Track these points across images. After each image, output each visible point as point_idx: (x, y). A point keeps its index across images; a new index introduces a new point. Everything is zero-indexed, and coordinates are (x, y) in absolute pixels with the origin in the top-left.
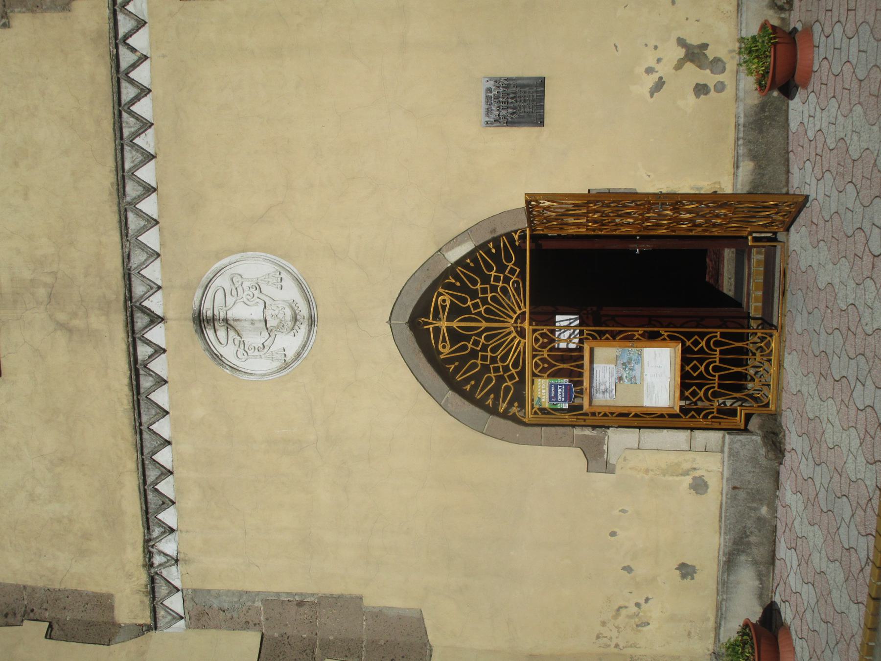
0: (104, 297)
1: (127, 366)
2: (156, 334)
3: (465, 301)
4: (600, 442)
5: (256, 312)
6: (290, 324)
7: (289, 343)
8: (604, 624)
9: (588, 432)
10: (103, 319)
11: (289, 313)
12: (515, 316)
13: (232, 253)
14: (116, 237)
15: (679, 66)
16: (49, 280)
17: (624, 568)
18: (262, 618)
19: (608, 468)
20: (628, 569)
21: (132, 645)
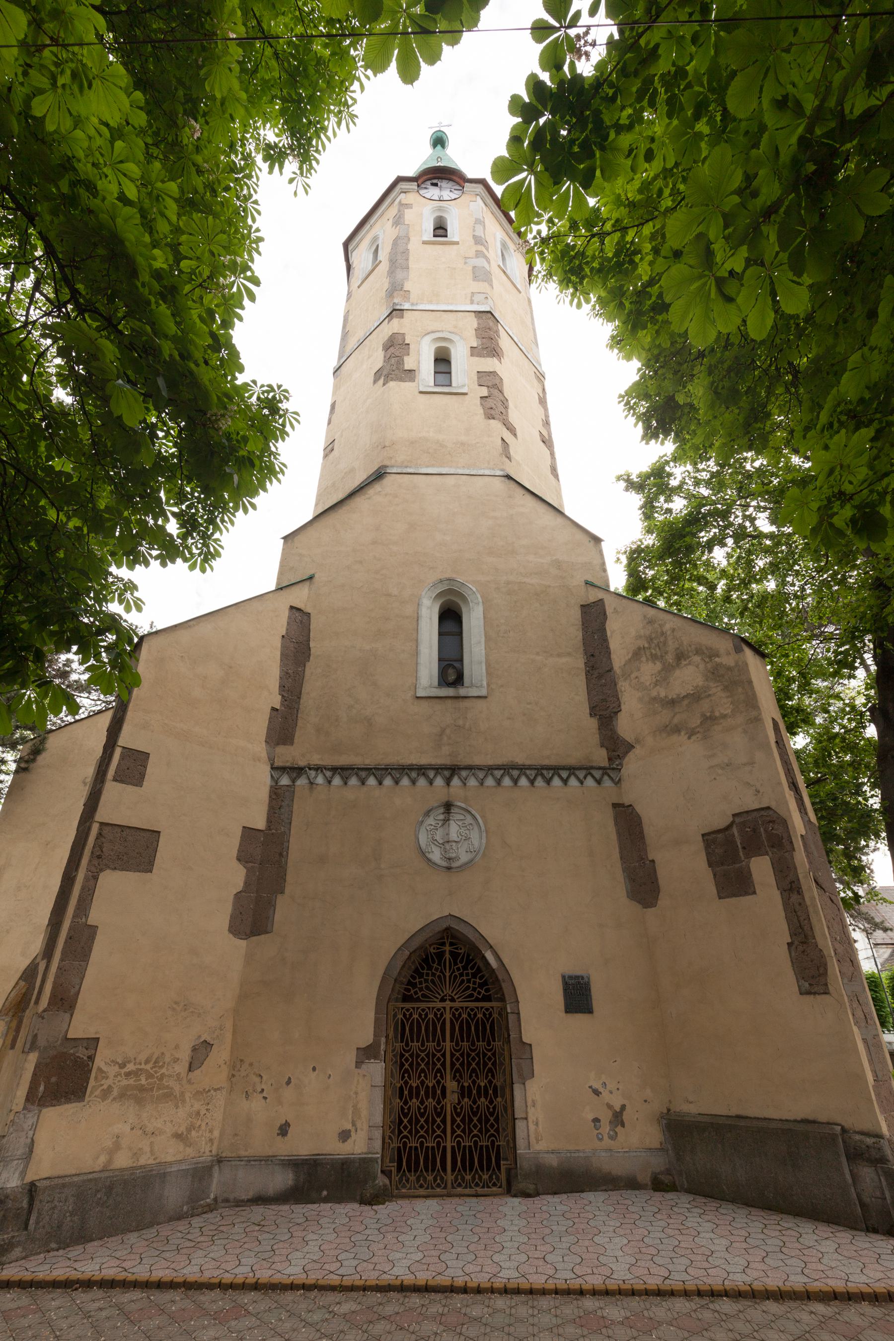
2: (439, 782)
3: (461, 962)
4: (376, 1057)
5: (454, 836)
7: (436, 855)
8: (251, 1064)
11: (454, 855)
13: (485, 824)
14: (490, 762)
15: (609, 1107)
19: (358, 1064)
20: (289, 1082)
21: (264, 755)
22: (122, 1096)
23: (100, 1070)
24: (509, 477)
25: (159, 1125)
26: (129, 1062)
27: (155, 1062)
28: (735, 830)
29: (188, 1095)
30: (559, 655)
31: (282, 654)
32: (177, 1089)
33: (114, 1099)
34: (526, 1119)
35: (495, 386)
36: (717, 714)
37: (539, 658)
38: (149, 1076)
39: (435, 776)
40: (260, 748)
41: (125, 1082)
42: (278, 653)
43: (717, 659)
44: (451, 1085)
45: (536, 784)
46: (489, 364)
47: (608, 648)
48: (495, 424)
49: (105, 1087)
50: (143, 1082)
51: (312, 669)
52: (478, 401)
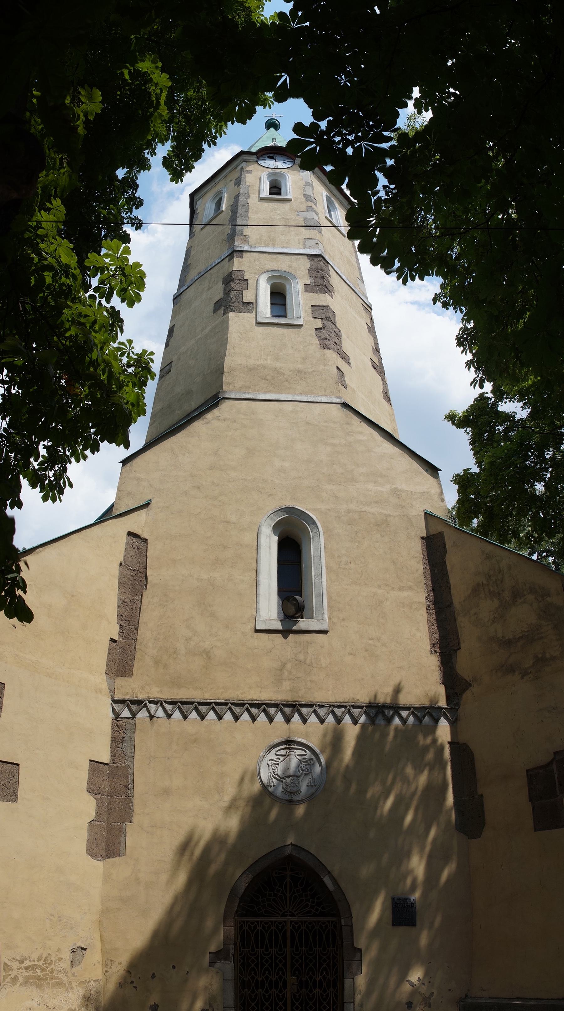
0: (300, 690)
1: (263, 699)
6: (289, 790)
9: (232, 951)
10: (288, 688)
12: (293, 911)
16: (308, 662)
17: (154, 974)
18: (118, 765)
20: (153, 976)
21: (105, 686)
22: (26, 982)
23: (5, 964)
24: (346, 406)
25: (58, 1003)
26: (26, 959)
27: (45, 960)
28: (554, 766)
29: (74, 984)
30: (401, 589)
31: (120, 583)
32: (65, 980)
33: (21, 984)
34: (353, 1002)
35: (328, 319)
36: (548, 656)
37: (380, 591)
38: (43, 970)
39: (276, 713)
40: (100, 680)
41: (26, 974)
42: (117, 581)
43: (549, 599)
44: (292, 980)
45: (377, 722)
46: (322, 299)
47: (448, 582)
48: (331, 354)
49: (13, 976)
50: (39, 973)
51: (150, 598)
52: (314, 332)
